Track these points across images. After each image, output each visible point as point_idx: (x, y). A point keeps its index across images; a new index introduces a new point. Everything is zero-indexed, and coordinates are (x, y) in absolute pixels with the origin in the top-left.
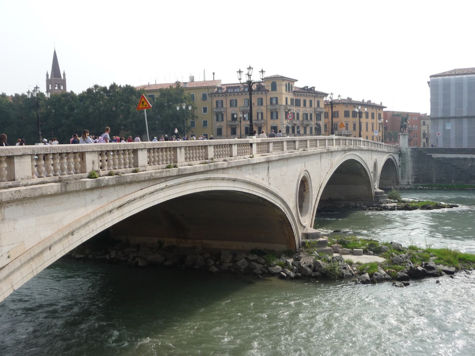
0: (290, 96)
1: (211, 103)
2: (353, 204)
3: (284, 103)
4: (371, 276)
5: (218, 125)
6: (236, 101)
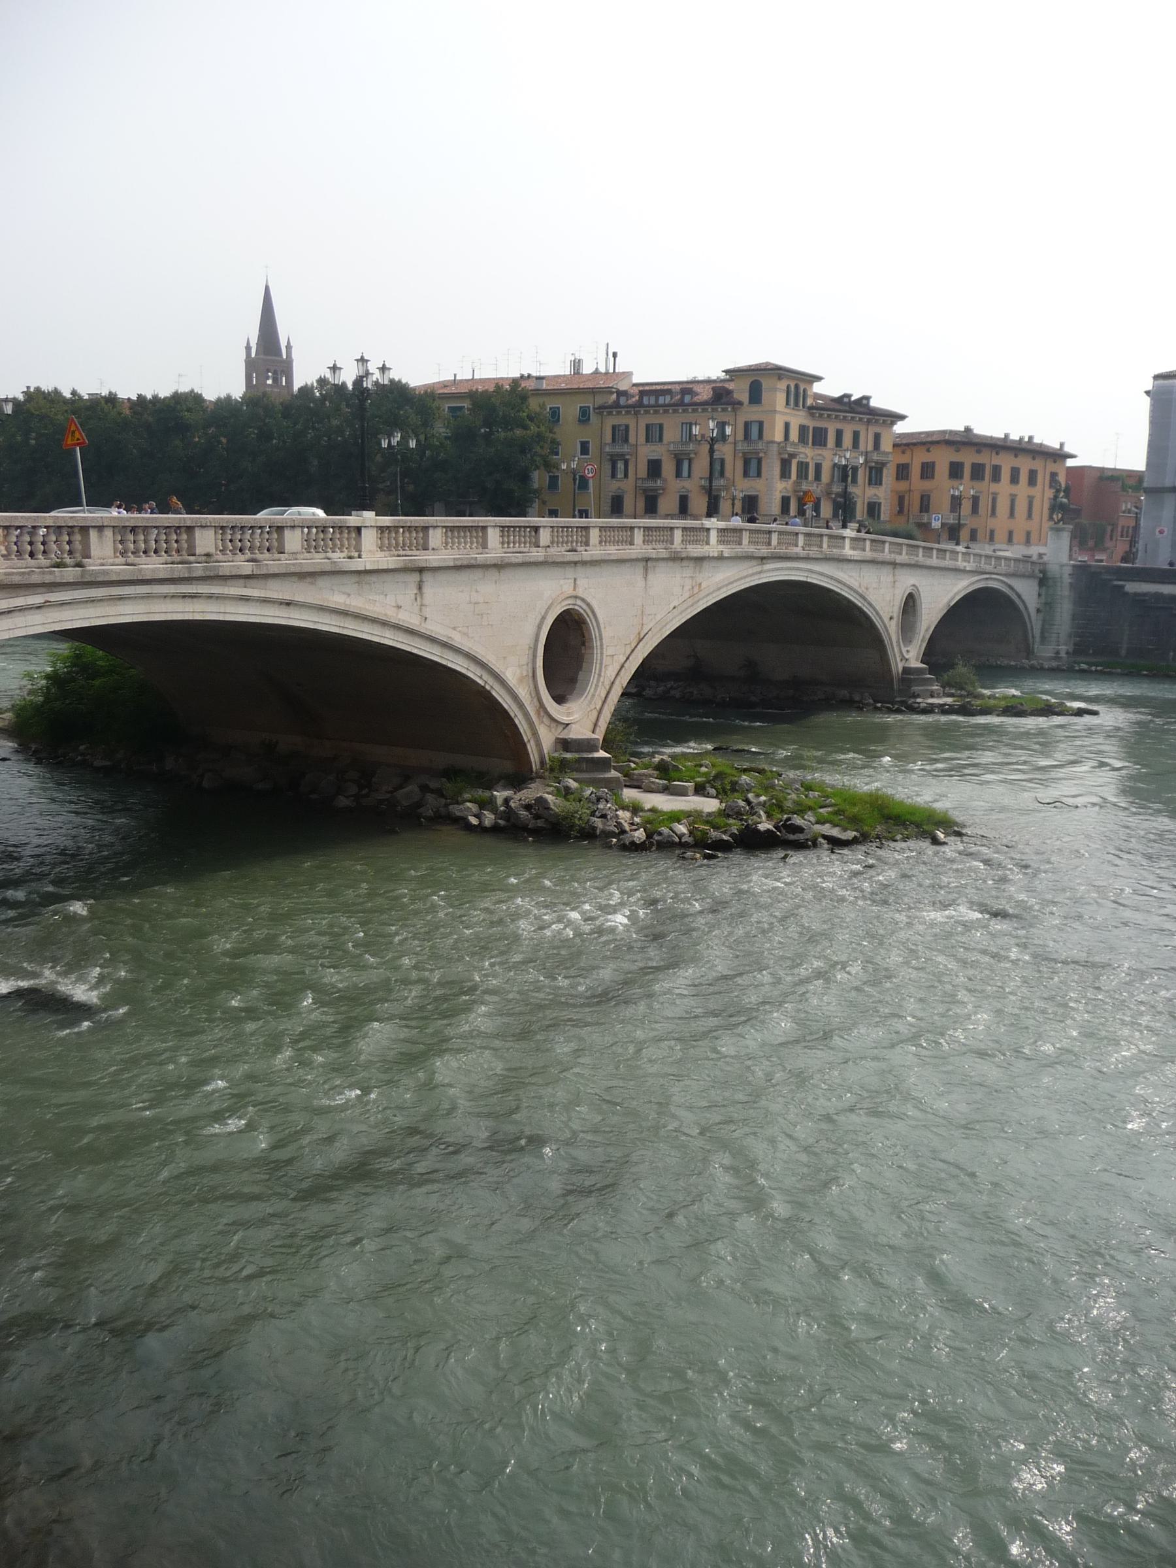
0: (798, 419)
1: (601, 431)
2: (844, 693)
3: (779, 437)
4: (649, 836)
5: (613, 486)
6: (661, 426)
